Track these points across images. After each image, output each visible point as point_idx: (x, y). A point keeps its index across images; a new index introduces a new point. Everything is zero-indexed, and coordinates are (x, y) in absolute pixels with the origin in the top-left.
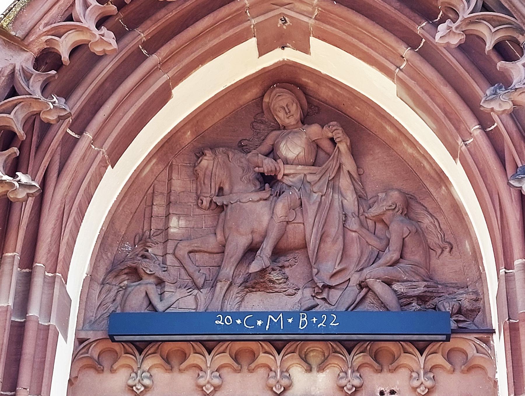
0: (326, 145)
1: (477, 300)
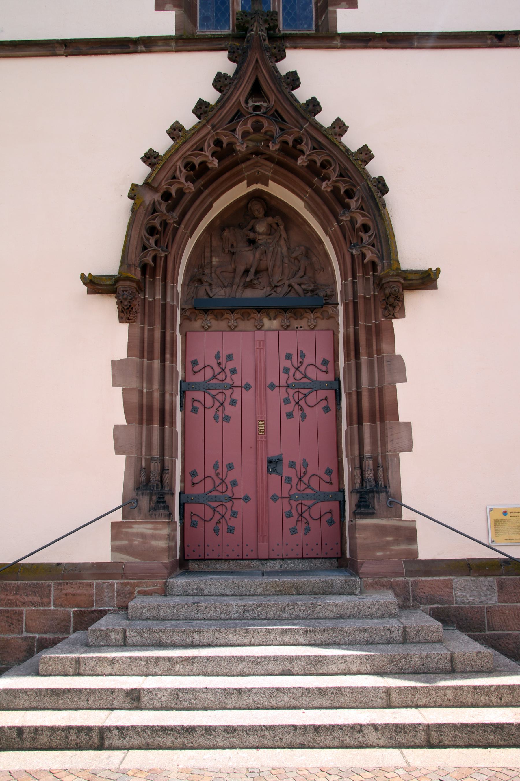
0: (275, 226)
1: (333, 291)
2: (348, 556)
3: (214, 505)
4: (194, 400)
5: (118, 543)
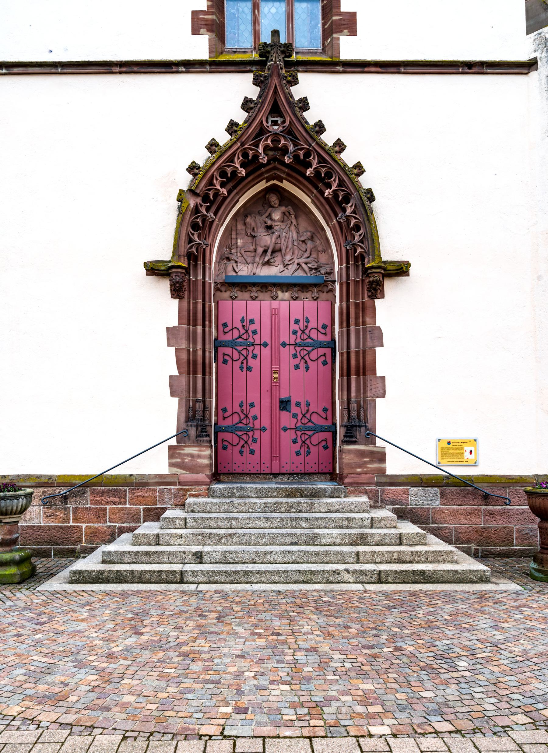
2: (338, 472)
3: (239, 433)
4: (224, 354)
5: (174, 461)
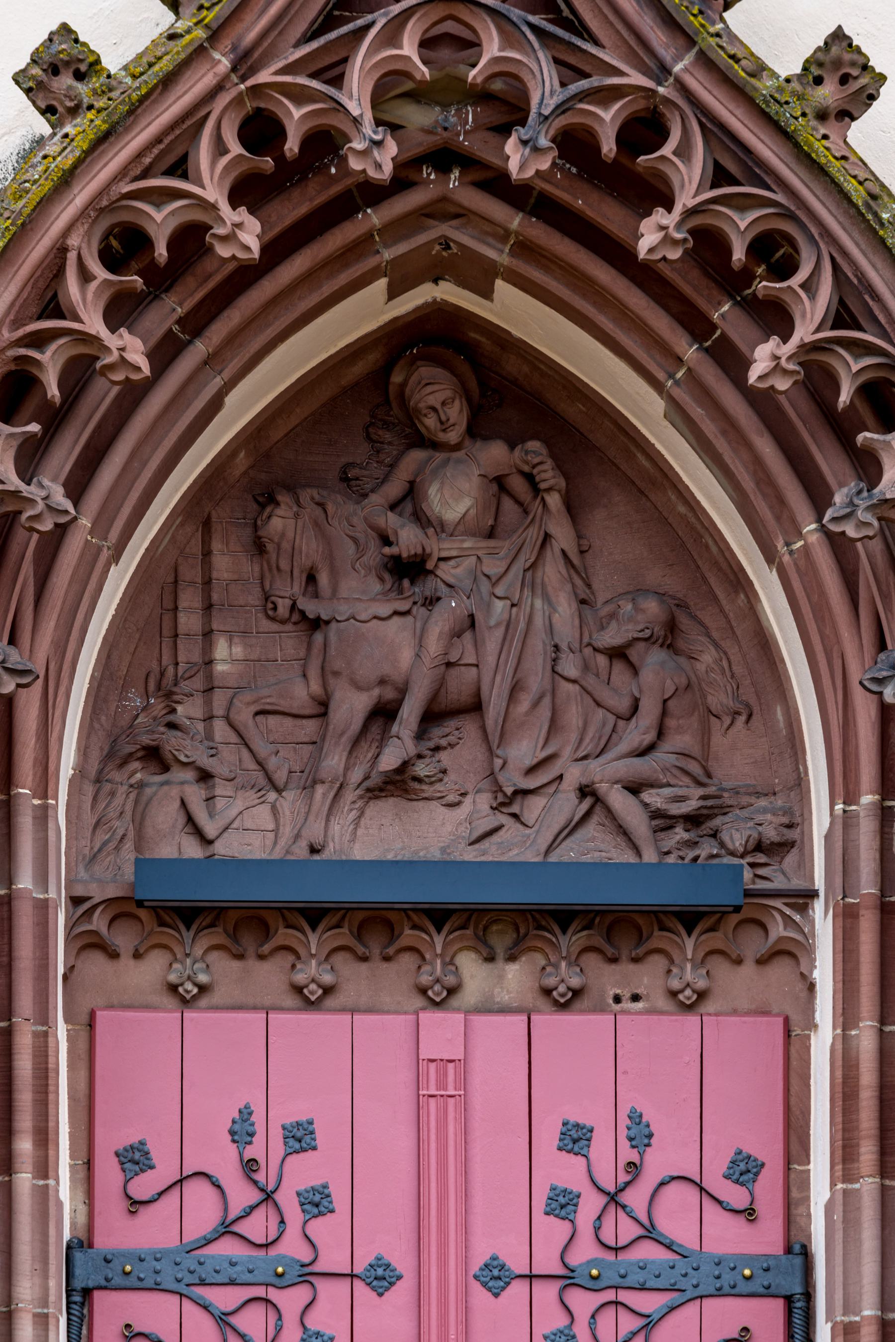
1: (790, 826)
